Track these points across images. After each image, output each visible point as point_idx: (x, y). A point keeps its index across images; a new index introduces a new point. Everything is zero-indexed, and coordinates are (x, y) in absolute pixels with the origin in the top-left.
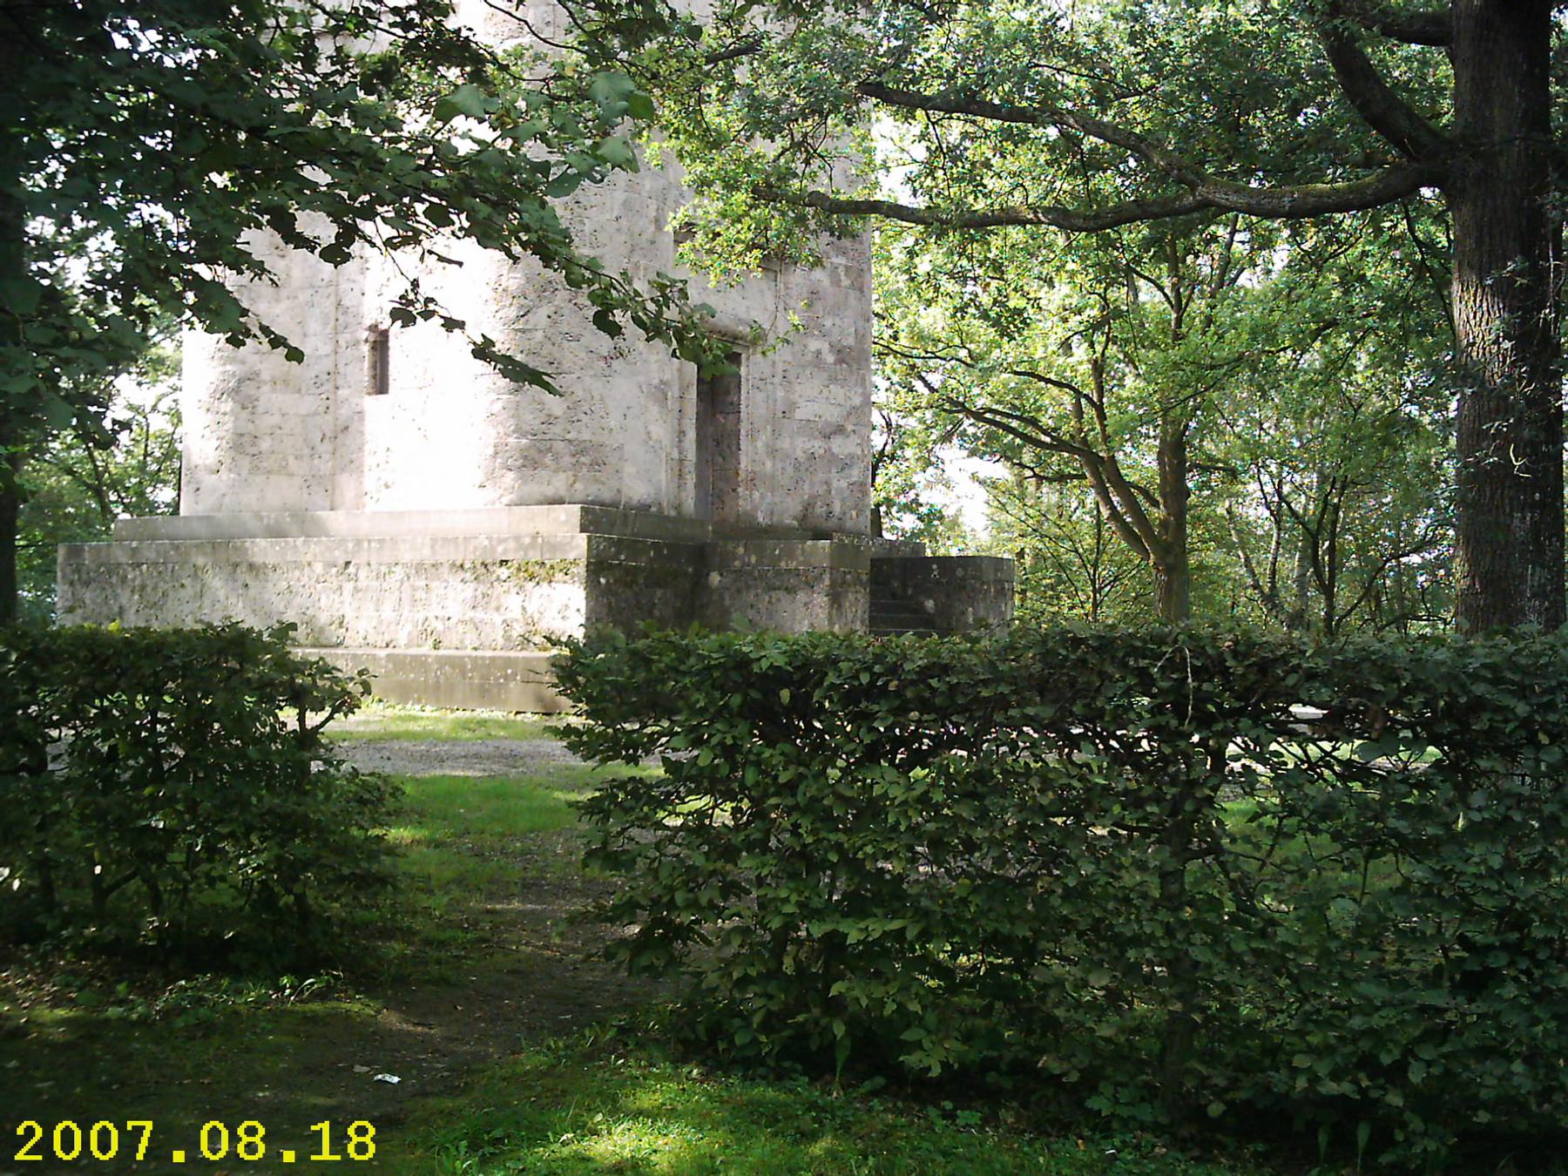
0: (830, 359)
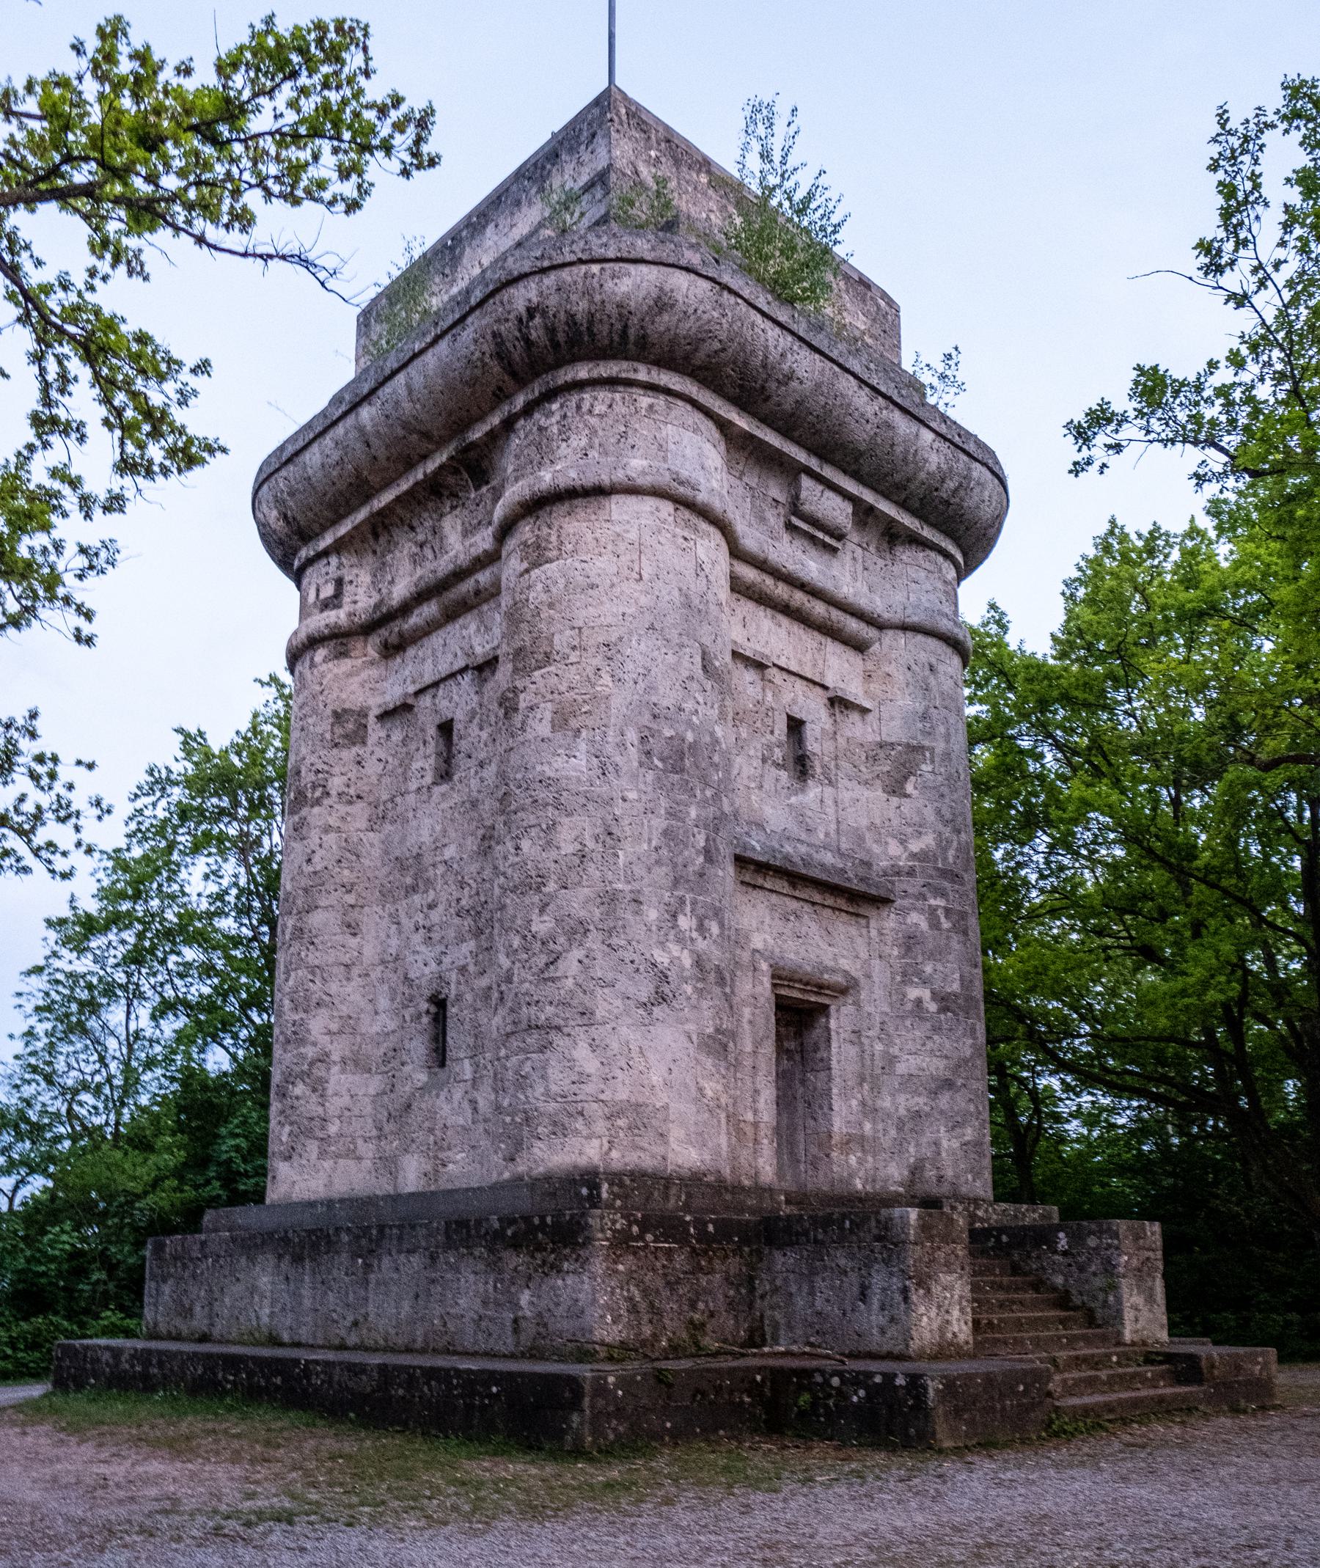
0: (933, 1007)
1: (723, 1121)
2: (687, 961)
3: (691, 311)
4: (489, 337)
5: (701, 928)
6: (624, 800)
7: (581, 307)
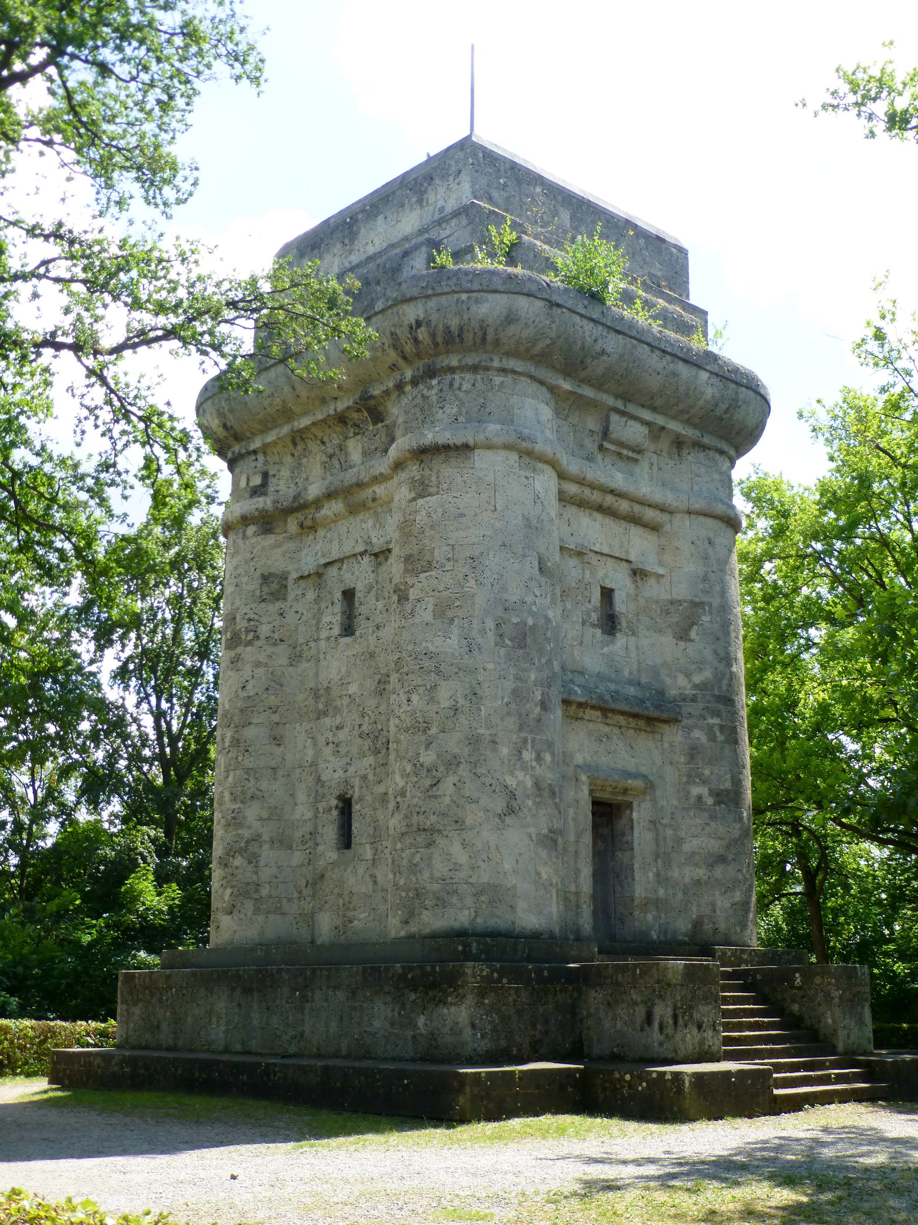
0: (710, 801)
1: (554, 895)
2: (529, 783)
3: (530, 322)
4: (388, 334)
5: (539, 759)
6: (485, 670)
7: (454, 323)
